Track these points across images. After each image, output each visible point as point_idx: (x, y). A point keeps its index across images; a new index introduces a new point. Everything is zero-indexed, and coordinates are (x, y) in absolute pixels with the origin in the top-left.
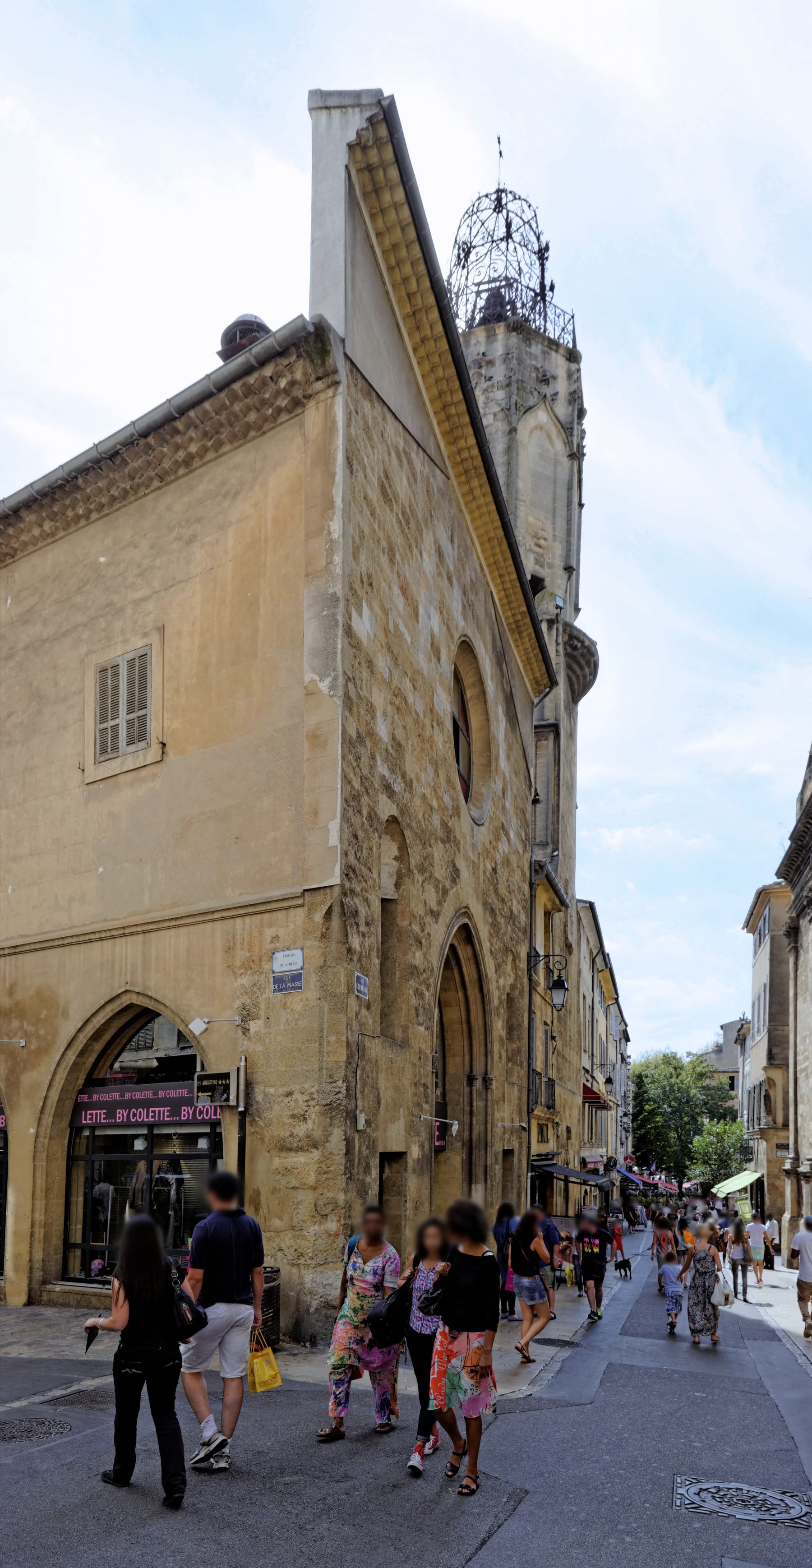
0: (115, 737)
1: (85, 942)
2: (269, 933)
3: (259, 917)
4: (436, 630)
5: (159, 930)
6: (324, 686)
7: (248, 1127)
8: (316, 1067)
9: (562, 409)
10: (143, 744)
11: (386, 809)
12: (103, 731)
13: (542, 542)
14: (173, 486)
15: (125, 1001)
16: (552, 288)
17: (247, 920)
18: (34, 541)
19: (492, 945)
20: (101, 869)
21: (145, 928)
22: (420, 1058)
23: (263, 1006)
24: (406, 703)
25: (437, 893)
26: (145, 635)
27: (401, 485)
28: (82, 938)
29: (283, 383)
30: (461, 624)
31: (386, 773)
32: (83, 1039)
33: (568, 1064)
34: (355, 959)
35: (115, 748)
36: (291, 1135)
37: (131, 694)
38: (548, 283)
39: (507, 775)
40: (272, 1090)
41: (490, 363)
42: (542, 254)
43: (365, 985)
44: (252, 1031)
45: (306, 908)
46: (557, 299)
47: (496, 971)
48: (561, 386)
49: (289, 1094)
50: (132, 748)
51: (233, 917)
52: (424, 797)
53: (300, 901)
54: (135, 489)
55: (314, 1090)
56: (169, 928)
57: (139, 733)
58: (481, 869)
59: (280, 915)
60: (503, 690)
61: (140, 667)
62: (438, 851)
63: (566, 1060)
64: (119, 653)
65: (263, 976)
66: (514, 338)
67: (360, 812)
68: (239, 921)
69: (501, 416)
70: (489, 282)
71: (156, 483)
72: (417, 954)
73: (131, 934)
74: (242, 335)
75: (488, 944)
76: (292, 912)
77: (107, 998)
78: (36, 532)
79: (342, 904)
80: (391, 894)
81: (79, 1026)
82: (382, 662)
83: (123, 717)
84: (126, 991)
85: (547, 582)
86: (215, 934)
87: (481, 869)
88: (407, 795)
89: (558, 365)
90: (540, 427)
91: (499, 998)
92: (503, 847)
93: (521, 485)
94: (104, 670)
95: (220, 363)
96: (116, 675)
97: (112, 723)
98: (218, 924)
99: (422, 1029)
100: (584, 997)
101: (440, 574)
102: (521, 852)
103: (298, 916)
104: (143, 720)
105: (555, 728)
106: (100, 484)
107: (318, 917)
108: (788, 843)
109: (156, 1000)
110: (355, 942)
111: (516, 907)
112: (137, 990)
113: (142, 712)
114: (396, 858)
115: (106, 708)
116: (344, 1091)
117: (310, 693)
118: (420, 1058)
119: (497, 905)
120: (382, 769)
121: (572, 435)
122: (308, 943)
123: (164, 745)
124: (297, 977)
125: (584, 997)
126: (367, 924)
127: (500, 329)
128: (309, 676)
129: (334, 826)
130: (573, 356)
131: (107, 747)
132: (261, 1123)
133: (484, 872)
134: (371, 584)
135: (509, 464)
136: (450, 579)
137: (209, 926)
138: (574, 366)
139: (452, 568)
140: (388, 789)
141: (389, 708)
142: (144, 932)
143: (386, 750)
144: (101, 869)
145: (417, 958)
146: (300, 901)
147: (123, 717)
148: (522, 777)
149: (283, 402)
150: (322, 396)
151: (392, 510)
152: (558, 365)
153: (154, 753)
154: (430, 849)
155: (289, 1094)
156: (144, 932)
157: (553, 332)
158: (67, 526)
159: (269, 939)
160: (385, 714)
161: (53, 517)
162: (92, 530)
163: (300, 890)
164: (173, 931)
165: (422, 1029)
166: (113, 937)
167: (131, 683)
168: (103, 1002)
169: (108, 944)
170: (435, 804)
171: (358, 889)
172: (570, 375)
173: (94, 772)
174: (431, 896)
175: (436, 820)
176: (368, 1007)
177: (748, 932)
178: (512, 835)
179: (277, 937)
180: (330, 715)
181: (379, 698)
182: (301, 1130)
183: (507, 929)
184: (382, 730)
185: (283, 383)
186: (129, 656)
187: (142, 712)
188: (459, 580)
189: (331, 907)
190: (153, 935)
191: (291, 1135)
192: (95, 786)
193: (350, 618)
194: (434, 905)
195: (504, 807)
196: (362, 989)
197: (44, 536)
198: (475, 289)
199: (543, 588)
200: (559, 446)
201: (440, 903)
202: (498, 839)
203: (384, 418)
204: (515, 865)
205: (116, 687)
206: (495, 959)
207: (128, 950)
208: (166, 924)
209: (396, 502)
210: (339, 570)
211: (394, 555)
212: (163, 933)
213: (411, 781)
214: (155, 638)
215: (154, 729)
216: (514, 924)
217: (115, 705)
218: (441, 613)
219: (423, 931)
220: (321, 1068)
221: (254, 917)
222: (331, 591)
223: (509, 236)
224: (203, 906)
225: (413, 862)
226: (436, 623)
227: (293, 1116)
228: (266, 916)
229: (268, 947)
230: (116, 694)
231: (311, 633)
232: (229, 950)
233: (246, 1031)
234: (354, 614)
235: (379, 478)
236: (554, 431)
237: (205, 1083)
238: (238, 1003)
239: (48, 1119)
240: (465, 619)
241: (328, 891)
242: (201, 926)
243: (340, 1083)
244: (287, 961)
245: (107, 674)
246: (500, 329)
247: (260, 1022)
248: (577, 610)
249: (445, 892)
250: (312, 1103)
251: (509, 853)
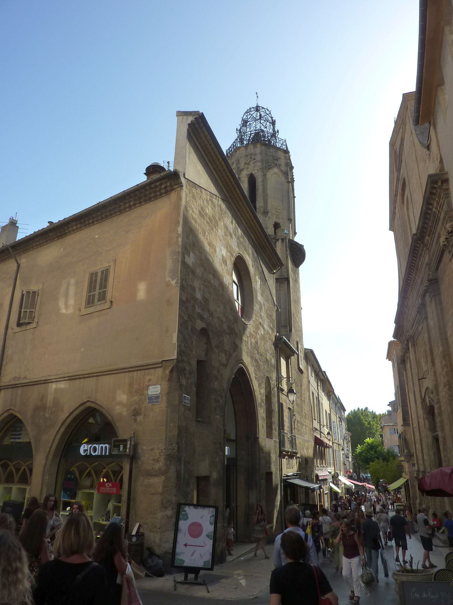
0: (93, 298)
1: (73, 379)
2: (148, 378)
3: (144, 371)
4: (224, 254)
5: (102, 375)
6: (173, 282)
7: (134, 464)
8: (164, 437)
9: (283, 168)
10: (103, 301)
11: (200, 325)
12: (89, 296)
13: (278, 211)
14: (123, 214)
15: (88, 405)
16: (278, 132)
17: (139, 372)
18: (73, 230)
19: (256, 375)
20: (83, 349)
21: (98, 374)
22: (217, 431)
23: (143, 410)
24: (210, 283)
25: (226, 356)
26: (109, 262)
27: (209, 211)
28: (72, 378)
29: (163, 187)
30: (236, 251)
31: (200, 311)
32: (69, 421)
33: (304, 427)
34: (184, 389)
35: (93, 302)
36: (153, 469)
37: (101, 283)
38: (276, 130)
39: (262, 302)
40: (145, 448)
41: (255, 154)
42: (273, 123)
43: (188, 400)
44: (138, 420)
45: (163, 368)
46: (280, 136)
47: (259, 387)
48: (282, 162)
49: (152, 450)
50: (100, 303)
51: (133, 371)
52: (219, 318)
53: (160, 365)
54: (111, 215)
55: (163, 448)
56: (107, 375)
57: (102, 297)
58: (249, 343)
59: (152, 370)
60: (259, 270)
61: (106, 273)
62: (226, 339)
63: (303, 425)
64: (99, 268)
65: (143, 397)
66: (264, 148)
67: (187, 329)
68: (135, 372)
69: (260, 170)
70: (255, 130)
71: (118, 213)
72: (215, 383)
73: (92, 377)
74: (153, 170)
75: (254, 375)
76: (157, 370)
77: (80, 404)
78: (75, 228)
79: (177, 367)
80: (203, 358)
81: (67, 415)
82: (199, 271)
83: (97, 291)
84: (88, 401)
85: (281, 224)
86: (126, 377)
87: (249, 343)
88: (211, 318)
89: (281, 155)
90: (275, 173)
91: (261, 399)
92: (262, 331)
93: (269, 192)
94: (92, 274)
95: (144, 178)
96: (96, 276)
97: (93, 293)
98: (127, 373)
99: (218, 417)
100: (313, 393)
101: (226, 235)
102: (271, 332)
103: (159, 371)
104: (104, 292)
105: (287, 280)
106: (98, 214)
107: (167, 372)
108: (394, 325)
109: (99, 405)
110: (184, 382)
111: (269, 357)
112: (92, 400)
113: (104, 290)
114: (206, 344)
115: (91, 287)
116: (176, 448)
117: (168, 285)
118: (217, 431)
119: (258, 357)
120: (198, 310)
121: (288, 176)
122: (163, 383)
123: (112, 302)
124: (157, 397)
125: (313, 393)
126: (190, 373)
127: (259, 145)
128: (168, 279)
129: (175, 335)
130: (287, 152)
131: (90, 302)
132: (140, 463)
133: (251, 344)
134: (194, 245)
135: (263, 185)
136: (231, 236)
137: (123, 375)
138: (287, 155)
139: (232, 232)
140: (201, 318)
141: (202, 286)
142: (97, 376)
143: (200, 302)
144: (83, 349)
145: (216, 385)
146: (160, 365)
147: (97, 291)
148: (270, 302)
149: (163, 191)
150: (177, 189)
151: (204, 219)
152: (281, 155)
153: (107, 305)
154: (222, 338)
155: (152, 450)
156: (97, 376)
157: (278, 145)
158: (85, 226)
159: (147, 380)
160: (200, 289)
161: (81, 223)
162: (94, 227)
163: (160, 360)
164: (108, 376)
165: (218, 417)
166: (85, 378)
167: (101, 279)
168: (78, 405)
169: (82, 380)
170: (224, 320)
171: (186, 359)
172: (286, 157)
173: (84, 311)
174: (223, 358)
175: (225, 326)
176: (189, 410)
177: (389, 360)
178: (265, 326)
179: (150, 380)
180: (175, 294)
181: (197, 284)
182: (157, 466)
183: (264, 367)
184: (199, 295)
185: (163, 187)
186: (102, 269)
187: (104, 290)
188: (235, 235)
189: (172, 368)
190: (101, 377)
191: (153, 469)
192: (84, 316)
193: (185, 259)
194: (224, 361)
195: (261, 315)
196: (187, 401)
197: (77, 229)
198: (249, 133)
199: (280, 227)
200: (283, 179)
201: (228, 360)
202: (258, 329)
203: (201, 192)
204: (268, 339)
205: (96, 280)
206: (258, 381)
207: (90, 383)
208: (106, 373)
209: (207, 216)
210: (180, 243)
211: (205, 233)
212: (105, 376)
213: (212, 312)
214: (112, 264)
215: (109, 296)
216: (268, 364)
217: (95, 287)
218: (227, 248)
219: (219, 373)
220: (166, 438)
221: (141, 371)
222: (177, 250)
223: (260, 119)
224: (122, 366)
225: (213, 344)
226: (224, 252)
227: (154, 460)
228: (146, 371)
229: (147, 384)
230: (96, 282)
231: (169, 264)
232: (131, 385)
233: (135, 420)
234: (186, 257)
235: (199, 210)
236: (281, 174)
237: (116, 444)
238: (133, 408)
239: (51, 457)
240: (238, 248)
241: (172, 361)
242: (120, 374)
243: (174, 445)
244: (154, 390)
245: (93, 276)
246: (259, 145)
247: (141, 417)
248: (295, 233)
249: (230, 355)
250: (162, 454)
251: (264, 334)
